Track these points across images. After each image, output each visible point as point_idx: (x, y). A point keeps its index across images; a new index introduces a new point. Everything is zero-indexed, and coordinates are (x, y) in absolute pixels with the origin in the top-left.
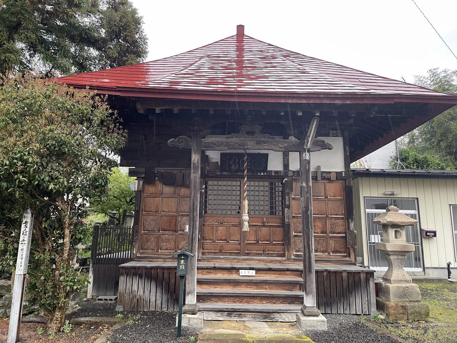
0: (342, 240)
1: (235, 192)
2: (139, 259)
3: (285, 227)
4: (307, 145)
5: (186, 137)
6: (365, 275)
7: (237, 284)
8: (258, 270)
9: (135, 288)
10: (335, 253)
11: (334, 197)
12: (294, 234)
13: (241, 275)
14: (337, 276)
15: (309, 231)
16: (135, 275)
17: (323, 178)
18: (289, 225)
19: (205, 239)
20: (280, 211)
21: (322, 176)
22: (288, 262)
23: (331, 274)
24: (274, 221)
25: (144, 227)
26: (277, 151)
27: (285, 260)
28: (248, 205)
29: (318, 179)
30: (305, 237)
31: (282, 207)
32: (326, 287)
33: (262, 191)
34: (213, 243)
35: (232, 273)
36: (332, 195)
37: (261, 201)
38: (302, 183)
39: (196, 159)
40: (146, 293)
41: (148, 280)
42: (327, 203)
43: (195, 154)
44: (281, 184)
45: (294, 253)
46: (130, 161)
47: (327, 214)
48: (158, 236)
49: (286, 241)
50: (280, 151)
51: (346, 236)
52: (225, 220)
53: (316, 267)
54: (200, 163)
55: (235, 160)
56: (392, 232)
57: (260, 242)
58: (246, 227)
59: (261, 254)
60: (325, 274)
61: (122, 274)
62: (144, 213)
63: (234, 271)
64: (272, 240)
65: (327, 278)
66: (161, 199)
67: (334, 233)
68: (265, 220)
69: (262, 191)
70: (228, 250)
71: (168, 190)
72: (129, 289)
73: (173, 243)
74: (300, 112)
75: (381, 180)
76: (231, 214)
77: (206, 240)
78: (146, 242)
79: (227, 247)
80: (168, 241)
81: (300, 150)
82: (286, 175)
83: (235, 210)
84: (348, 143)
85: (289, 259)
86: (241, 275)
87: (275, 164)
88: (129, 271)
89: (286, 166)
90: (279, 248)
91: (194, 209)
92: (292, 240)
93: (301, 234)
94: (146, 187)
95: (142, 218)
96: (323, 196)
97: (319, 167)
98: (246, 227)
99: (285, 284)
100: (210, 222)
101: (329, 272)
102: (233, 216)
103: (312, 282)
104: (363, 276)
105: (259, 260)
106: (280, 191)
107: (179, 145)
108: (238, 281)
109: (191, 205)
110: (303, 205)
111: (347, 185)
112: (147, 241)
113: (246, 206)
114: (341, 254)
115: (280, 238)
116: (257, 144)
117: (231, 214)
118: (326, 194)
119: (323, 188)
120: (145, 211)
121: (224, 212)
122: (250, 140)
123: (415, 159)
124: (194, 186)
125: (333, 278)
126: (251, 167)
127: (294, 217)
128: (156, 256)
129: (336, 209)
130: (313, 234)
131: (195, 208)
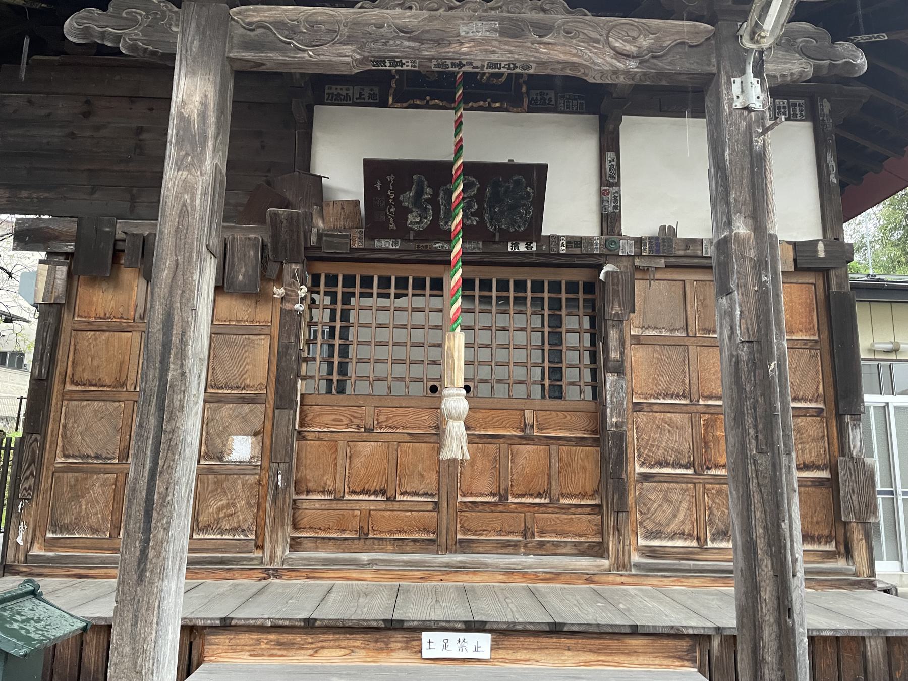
0: (823, 493)
3: (606, 445)
12: (639, 469)
13: (426, 654)
15: (775, 465)
18: (621, 437)
20: (586, 384)
22: (619, 579)
24: (567, 423)
28: (467, 363)
30: (756, 498)
34: (334, 505)
35: (387, 649)
37: (517, 347)
39: (197, 98)
43: (192, 73)
45: (642, 542)
46: (24, 194)
49: (611, 493)
51: (833, 483)
52: (382, 418)
54: (212, 119)
55: (420, 192)
58: (456, 444)
59: (516, 545)
62: (69, 387)
63: (399, 636)
64: (555, 492)
68: (529, 414)
70: (391, 532)
76: (407, 396)
82: (612, 255)
83: (421, 380)
85: (621, 565)
86: (426, 654)
87: (569, 214)
89: (610, 220)
90: (584, 521)
91: (166, 346)
98: (456, 444)
102: (413, 403)
105: (510, 572)
107: (118, 38)
112: (77, 497)
114: (816, 547)
115: (589, 485)
116: (503, 32)
117: (407, 396)
120: (73, 382)
121: (381, 388)
122: (471, 18)
124: (177, 230)
126: (482, 222)
128: (107, 555)
130: (797, 474)
131: (175, 340)
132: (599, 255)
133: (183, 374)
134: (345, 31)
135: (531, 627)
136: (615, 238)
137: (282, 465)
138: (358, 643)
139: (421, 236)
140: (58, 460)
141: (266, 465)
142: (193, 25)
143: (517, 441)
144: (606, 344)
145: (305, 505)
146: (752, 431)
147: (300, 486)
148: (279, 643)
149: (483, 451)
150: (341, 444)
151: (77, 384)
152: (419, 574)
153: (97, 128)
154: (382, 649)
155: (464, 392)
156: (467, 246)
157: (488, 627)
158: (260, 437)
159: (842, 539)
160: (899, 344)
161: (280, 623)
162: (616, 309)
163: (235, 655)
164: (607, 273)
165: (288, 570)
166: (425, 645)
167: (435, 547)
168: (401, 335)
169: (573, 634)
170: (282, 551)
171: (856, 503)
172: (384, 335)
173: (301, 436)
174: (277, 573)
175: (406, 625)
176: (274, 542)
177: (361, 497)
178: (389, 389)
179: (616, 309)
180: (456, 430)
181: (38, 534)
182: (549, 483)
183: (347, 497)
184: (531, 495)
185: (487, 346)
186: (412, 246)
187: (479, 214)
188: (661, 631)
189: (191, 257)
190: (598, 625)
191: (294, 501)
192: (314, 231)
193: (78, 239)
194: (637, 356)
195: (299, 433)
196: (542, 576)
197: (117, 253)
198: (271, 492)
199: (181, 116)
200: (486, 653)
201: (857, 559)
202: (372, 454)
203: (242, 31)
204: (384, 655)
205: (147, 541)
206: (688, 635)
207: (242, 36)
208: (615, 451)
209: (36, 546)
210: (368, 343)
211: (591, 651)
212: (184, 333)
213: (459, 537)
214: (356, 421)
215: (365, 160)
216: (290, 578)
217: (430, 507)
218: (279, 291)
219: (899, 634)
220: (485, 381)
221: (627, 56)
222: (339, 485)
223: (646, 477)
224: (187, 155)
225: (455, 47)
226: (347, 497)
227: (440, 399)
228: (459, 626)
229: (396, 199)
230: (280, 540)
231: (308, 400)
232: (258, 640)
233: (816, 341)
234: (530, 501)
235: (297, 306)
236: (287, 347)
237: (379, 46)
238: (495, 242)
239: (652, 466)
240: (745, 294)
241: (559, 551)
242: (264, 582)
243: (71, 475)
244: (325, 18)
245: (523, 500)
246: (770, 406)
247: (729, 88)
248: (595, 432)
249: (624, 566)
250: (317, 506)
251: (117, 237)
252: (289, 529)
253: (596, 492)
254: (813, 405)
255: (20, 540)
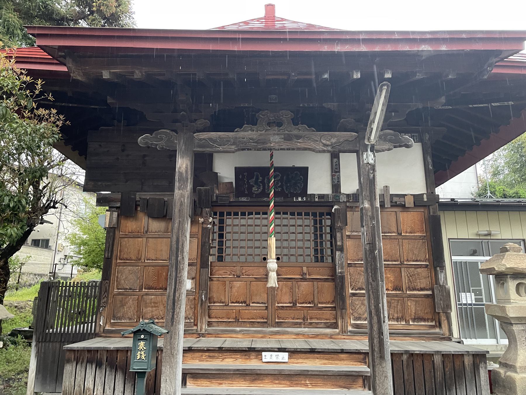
0: (428, 301)
1: (263, 231)
2: (107, 334)
3: (337, 281)
4: (369, 139)
5: (168, 131)
6: (471, 358)
7: (256, 377)
8: (293, 353)
9: (89, 384)
10: (418, 322)
11: (411, 232)
12: (351, 291)
14: (426, 362)
15: (378, 285)
16: (90, 361)
17: (394, 204)
18: (342, 278)
19: (212, 301)
21: (391, 202)
22: (343, 337)
23: (415, 357)
24: (320, 272)
25: (119, 283)
26: (320, 152)
27: (338, 334)
29: (386, 206)
31: (332, 250)
32: (408, 380)
33: (300, 226)
34: (225, 308)
35: (249, 358)
36: (408, 231)
37: (299, 240)
38: (363, 203)
39: (184, 166)
40: (108, 392)
41: (111, 371)
42: (400, 243)
43: (182, 157)
44: (327, 213)
45: (353, 322)
46: (100, 183)
47: (402, 260)
48: (140, 298)
49: (339, 302)
50: (324, 151)
51: (432, 296)
52: (244, 271)
53: (393, 345)
54: (189, 173)
55: (257, 178)
56: (512, 285)
57: (298, 305)
58: (273, 281)
59: (300, 324)
60: (405, 357)
61: (69, 361)
62: (118, 261)
63: (253, 354)
64: (316, 301)
65: (408, 365)
66: (145, 239)
67: (414, 289)
68: (305, 269)
69: (300, 226)
70: (248, 319)
71: (156, 225)
72: (80, 386)
73: (162, 307)
74: (357, 72)
75: (471, 215)
76: (254, 262)
77: (214, 303)
78: (120, 307)
79: (246, 313)
80: (155, 304)
81: (358, 149)
83: (259, 255)
84: (430, 150)
85: (344, 332)
87: (319, 184)
88: (80, 355)
89: (336, 186)
90: (328, 314)
91: (177, 249)
92: (348, 301)
93: (364, 292)
94: (123, 222)
95: (115, 270)
96: (394, 232)
97: (386, 188)
98: (273, 281)
99: (338, 377)
100: (221, 275)
101: (411, 355)
102: (256, 265)
103: (386, 377)
104: (468, 361)
105: (297, 334)
106: (328, 226)
107: (157, 145)
108: (259, 372)
109: (174, 243)
110: (365, 240)
111: (431, 214)
112: (123, 306)
113: (272, 246)
114: (426, 324)
116: (285, 139)
118: (399, 228)
119: (394, 220)
120: (120, 259)
121: (243, 259)
122: (274, 134)
123: (504, 195)
124: (179, 210)
125: (418, 364)
126: (283, 189)
127: (350, 265)
129: (416, 252)
130: (386, 292)
131: (180, 247)
132: (332, 202)
133: (183, 258)
134: (232, 141)
135: (303, 350)
136: (338, 194)
137: (204, 291)
138: (238, 356)
139: (258, 196)
140: (115, 291)
141: (197, 292)
142: (182, 141)
143: (300, 280)
144: (335, 239)
145: (213, 308)
146: (370, 274)
147: (210, 300)
148: (210, 357)
149: (286, 285)
150: (227, 283)
151: (121, 260)
152: (260, 335)
153: (128, 156)
154: (247, 359)
155: (275, 261)
156: (277, 199)
157: (287, 350)
158: (194, 280)
159: (437, 320)
160: (491, 231)
161: (210, 349)
162: (339, 224)
163: (193, 361)
164: (335, 209)
165: (208, 334)
166: (263, 357)
167: (267, 325)
168: (250, 236)
169: (319, 352)
170: (205, 327)
171: (442, 305)
172: (243, 236)
173: (211, 279)
174: (203, 335)
175: (256, 349)
176: (202, 323)
177: (236, 305)
178: (246, 259)
179: (339, 224)
180: (273, 276)
181: (108, 321)
182: (314, 298)
183: (230, 304)
184: (306, 303)
185: (287, 240)
186: (255, 200)
187: (281, 186)
188: (352, 351)
189: (184, 219)
190: (328, 349)
191: (209, 306)
192: (215, 195)
193: (122, 201)
194: (349, 244)
195: (210, 278)
196: (311, 336)
197: (137, 206)
198: (200, 303)
199: (179, 172)
200: (286, 360)
201: (443, 328)
202: (240, 286)
203: (197, 141)
204: (248, 361)
205: (174, 312)
206: (363, 353)
207: (198, 143)
208: (340, 284)
209: (107, 325)
210: (237, 240)
211: (326, 359)
212: (183, 244)
213: (277, 320)
214: (233, 273)
215: (236, 168)
216: (209, 337)
217: (264, 308)
218: (201, 220)
219: (446, 353)
220: (286, 255)
221: (327, 145)
222: (227, 300)
223: (354, 295)
224: (182, 185)
225: (269, 145)
226: (230, 304)
227: (267, 263)
228: (276, 350)
229: (248, 182)
230: (204, 322)
231: (213, 265)
232: (202, 355)
233: (425, 236)
234: (306, 305)
235: (209, 226)
236: (205, 243)
237: (243, 145)
238: (288, 197)
239: (356, 290)
240: (368, 227)
241: (318, 326)
242: (198, 339)
243: (120, 296)
244: (225, 136)
245: (303, 305)
246: (376, 265)
247: (363, 156)
248: (332, 276)
249: (345, 332)
250: (218, 308)
251: (137, 200)
252: (207, 317)
253: (333, 301)
254: (424, 263)
255: (101, 323)
